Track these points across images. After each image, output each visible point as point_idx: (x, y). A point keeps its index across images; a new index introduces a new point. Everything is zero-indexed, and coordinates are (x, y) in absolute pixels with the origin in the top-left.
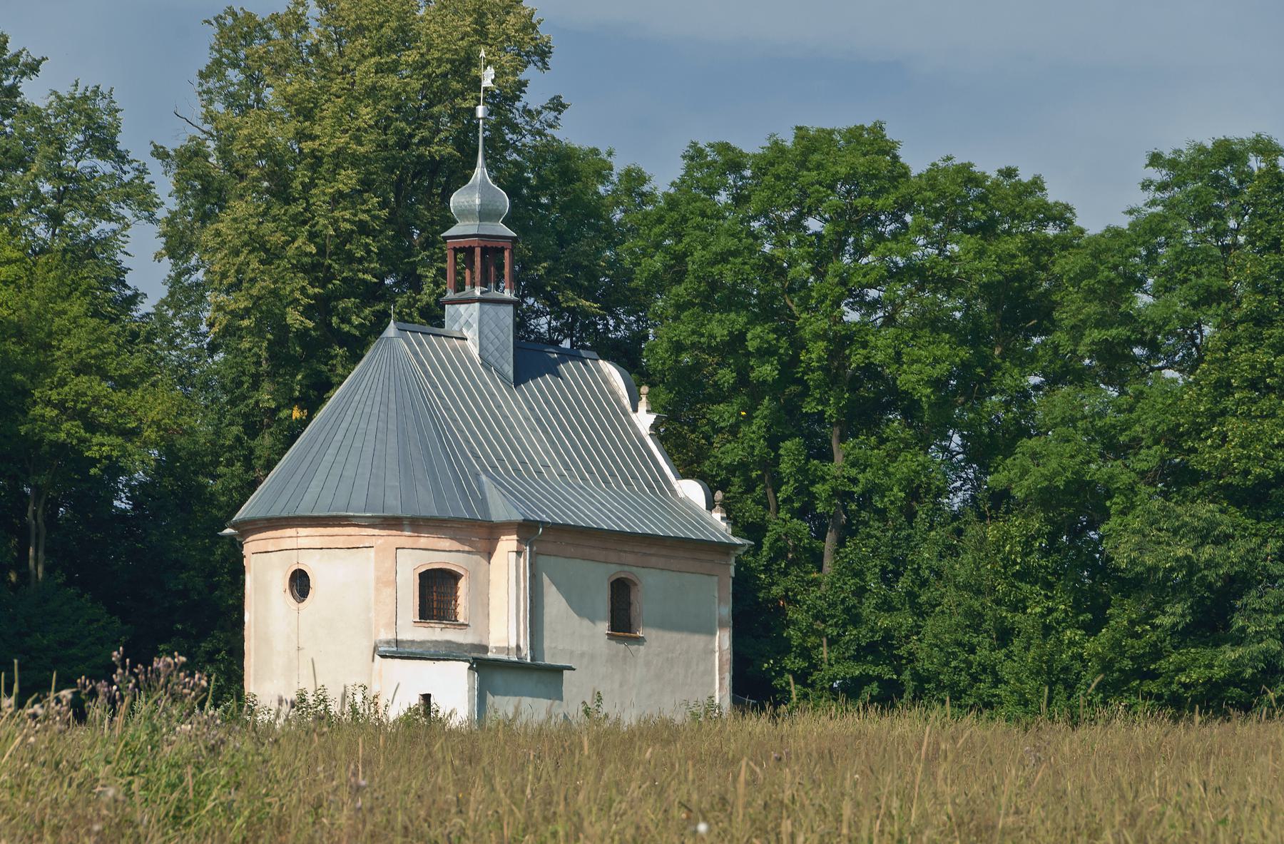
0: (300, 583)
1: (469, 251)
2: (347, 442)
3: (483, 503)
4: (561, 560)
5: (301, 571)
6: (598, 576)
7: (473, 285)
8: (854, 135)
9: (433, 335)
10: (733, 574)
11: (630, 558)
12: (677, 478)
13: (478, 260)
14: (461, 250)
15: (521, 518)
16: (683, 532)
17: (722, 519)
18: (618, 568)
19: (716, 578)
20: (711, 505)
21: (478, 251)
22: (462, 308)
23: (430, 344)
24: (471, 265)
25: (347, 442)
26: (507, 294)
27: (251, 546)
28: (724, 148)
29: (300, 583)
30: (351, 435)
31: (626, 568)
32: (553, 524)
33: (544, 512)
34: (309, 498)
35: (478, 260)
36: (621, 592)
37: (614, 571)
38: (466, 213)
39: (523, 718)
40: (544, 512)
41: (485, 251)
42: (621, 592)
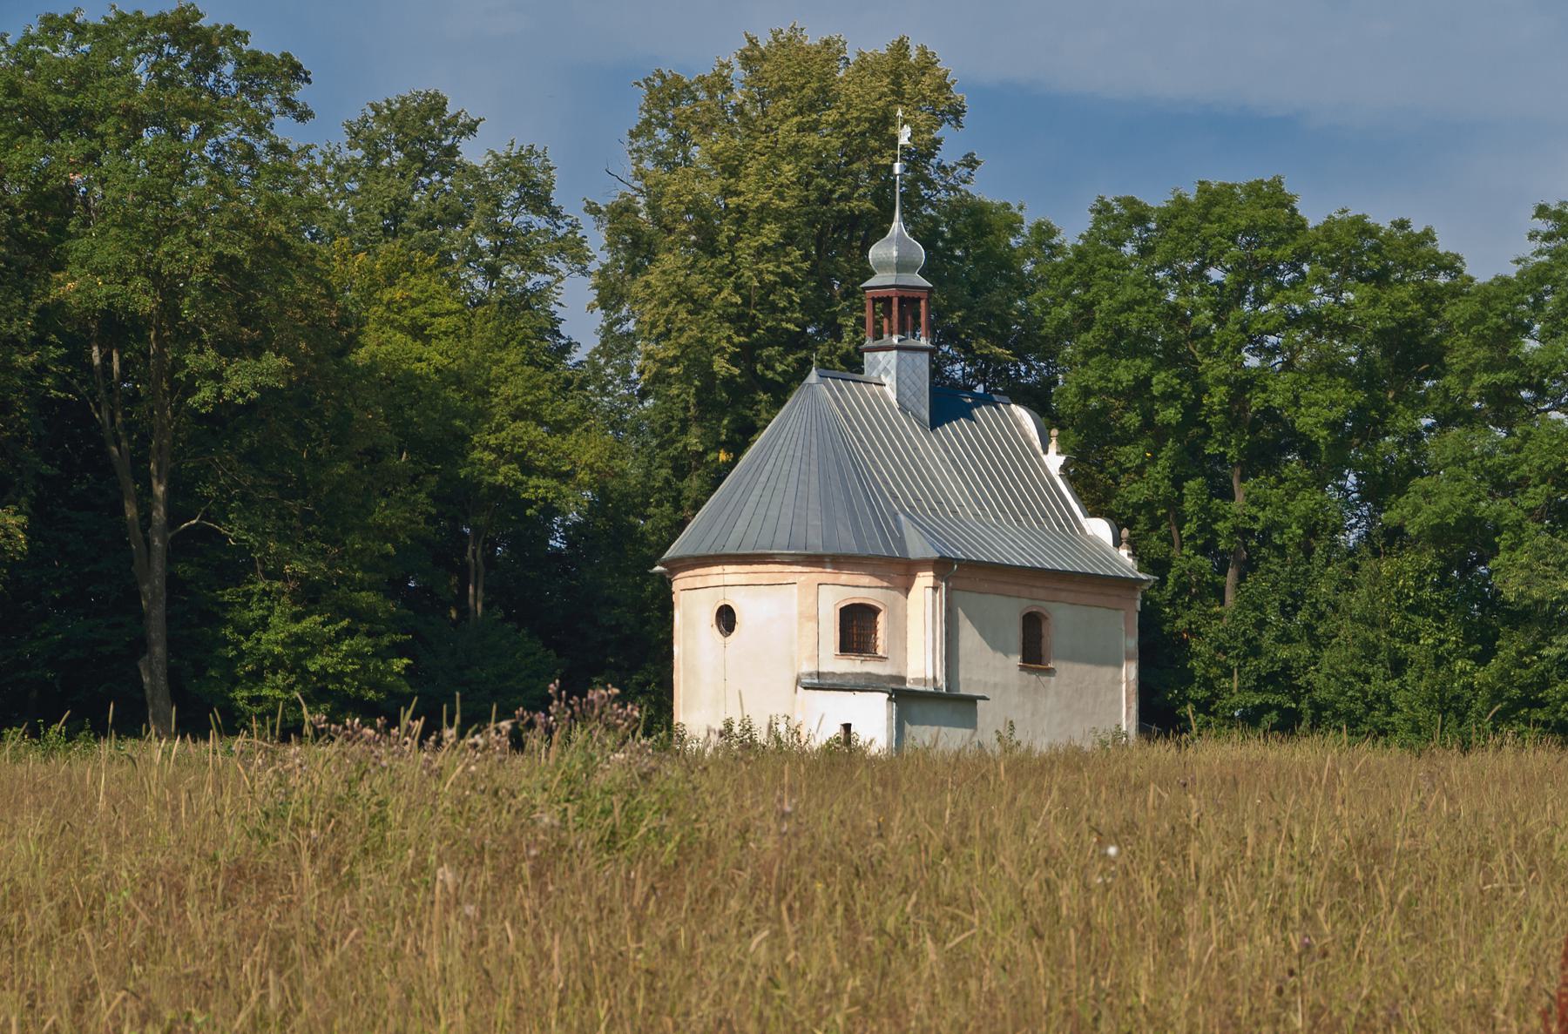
0: (726, 618)
1: (887, 301)
3: (901, 542)
6: (1010, 611)
12: (1085, 516)
13: (895, 309)
20: (1117, 542)
21: (895, 300)
22: (880, 355)
27: (680, 583)
28: (1130, 202)
29: (726, 618)
31: (1037, 603)
35: (895, 309)
36: (1033, 626)
38: (884, 265)
41: (902, 300)
42: (1033, 626)
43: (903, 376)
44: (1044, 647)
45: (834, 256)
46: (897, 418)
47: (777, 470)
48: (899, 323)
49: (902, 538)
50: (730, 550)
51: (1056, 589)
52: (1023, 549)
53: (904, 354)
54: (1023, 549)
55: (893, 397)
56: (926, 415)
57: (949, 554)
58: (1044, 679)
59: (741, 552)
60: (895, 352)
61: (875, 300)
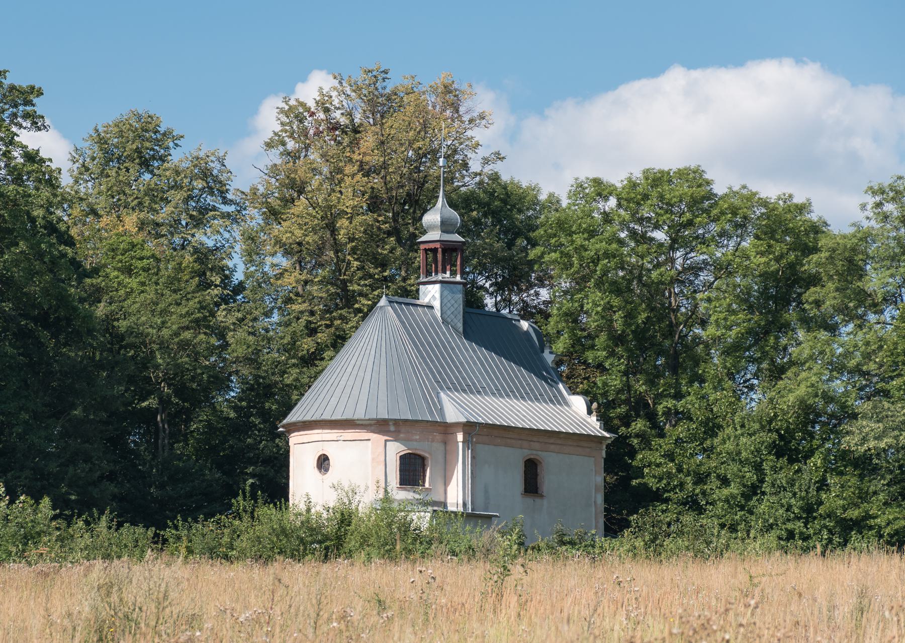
0: (323, 462)
1: (435, 251)
2: (355, 372)
3: (441, 411)
4: (492, 447)
5: (324, 455)
6: (516, 457)
7: (436, 273)
8: (682, 174)
9: (397, 302)
10: (604, 455)
11: (536, 445)
12: (569, 394)
13: (440, 256)
14: (430, 250)
15: (464, 420)
16: (506, 422)
17: (597, 420)
18: (529, 452)
19: (593, 459)
20: (590, 412)
21: (440, 250)
22: (430, 287)
23: (402, 310)
24: (435, 260)
25: (355, 372)
26: (458, 278)
27: (294, 439)
28: (597, 182)
29: (323, 462)
30: (356, 368)
31: (534, 452)
32: (566, 433)
33: (480, 416)
34: (340, 408)
35: (440, 256)
36: (532, 470)
37: (527, 453)
38: (432, 227)
39: (647, 570)
40: (480, 416)
41: (444, 251)
42: (532, 470)
43: (445, 308)
44: (539, 481)
45: (331, 214)
46: (440, 328)
47: (358, 363)
48: (472, 473)
49: (442, 409)
50: (327, 417)
51: (546, 443)
52: (525, 416)
53: (445, 285)
54: (525, 416)
55: (439, 314)
56: (460, 326)
57: (473, 420)
58: (538, 500)
59: (333, 418)
60: (438, 286)
61: (426, 250)
